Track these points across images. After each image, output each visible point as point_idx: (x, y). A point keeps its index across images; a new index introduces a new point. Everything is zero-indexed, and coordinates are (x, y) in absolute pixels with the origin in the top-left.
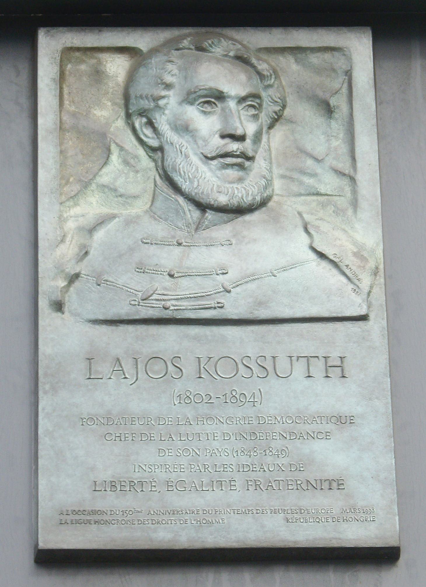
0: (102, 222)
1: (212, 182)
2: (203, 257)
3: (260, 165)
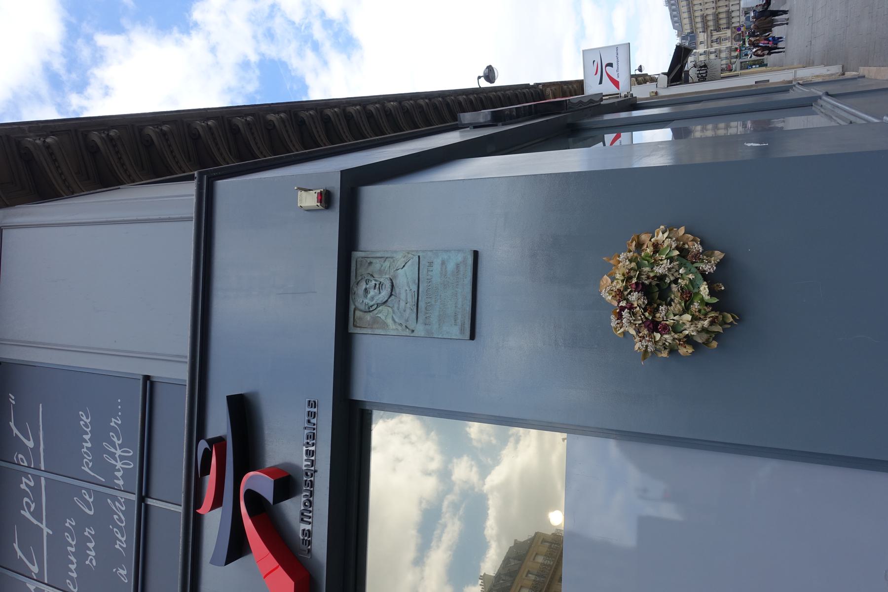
0: (393, 320)
1: (385, 293)
2: (403, 296)
3: (382, 280)
